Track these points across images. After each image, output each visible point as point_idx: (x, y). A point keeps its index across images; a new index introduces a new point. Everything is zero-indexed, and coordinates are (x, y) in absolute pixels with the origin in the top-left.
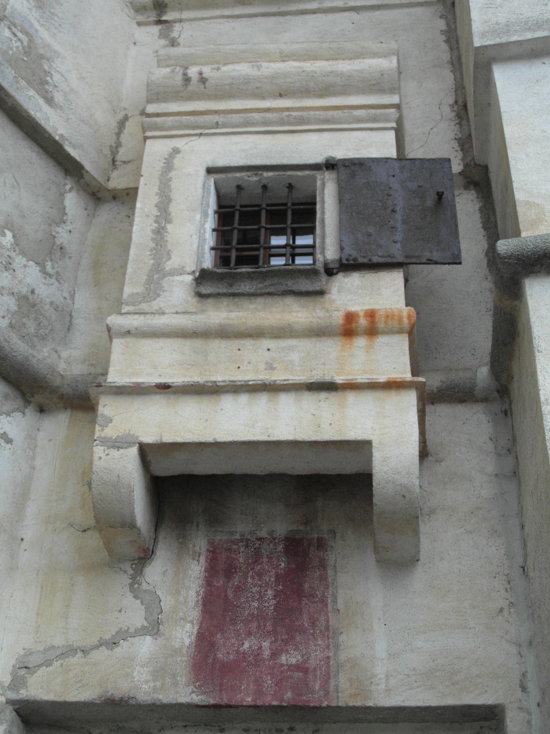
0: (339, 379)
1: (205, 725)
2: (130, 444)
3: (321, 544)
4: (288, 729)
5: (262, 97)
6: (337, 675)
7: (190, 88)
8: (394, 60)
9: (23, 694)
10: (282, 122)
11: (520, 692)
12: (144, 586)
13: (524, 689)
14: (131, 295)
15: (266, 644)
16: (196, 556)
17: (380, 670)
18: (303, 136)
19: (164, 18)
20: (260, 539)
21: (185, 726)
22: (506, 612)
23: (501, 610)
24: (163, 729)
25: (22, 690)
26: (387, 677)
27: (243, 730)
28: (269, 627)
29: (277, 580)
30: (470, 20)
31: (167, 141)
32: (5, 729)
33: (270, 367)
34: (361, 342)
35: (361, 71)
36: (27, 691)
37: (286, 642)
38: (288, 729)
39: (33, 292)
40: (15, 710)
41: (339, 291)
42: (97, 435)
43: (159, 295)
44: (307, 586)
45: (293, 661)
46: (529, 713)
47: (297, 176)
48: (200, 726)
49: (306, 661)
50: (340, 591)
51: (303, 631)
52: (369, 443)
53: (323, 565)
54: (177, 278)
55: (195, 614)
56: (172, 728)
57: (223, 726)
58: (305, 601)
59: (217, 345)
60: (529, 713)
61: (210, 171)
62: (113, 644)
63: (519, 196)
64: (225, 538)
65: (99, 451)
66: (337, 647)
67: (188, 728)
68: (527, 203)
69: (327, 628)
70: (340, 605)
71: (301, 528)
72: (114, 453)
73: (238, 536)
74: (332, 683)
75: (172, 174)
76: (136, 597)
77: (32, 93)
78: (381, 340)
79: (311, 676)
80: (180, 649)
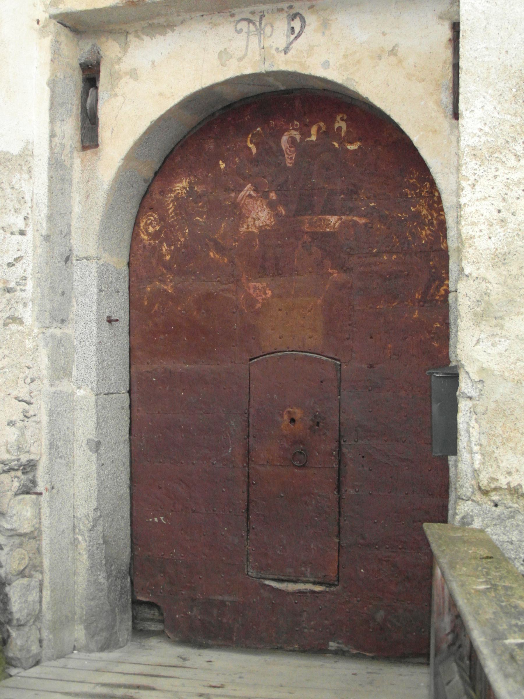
1: (218, 13)
4: (288, 8)
11: (291, 51)
21: (202, 16)
24: (184, 20)
25: (61, 5)
27: (250, 13)
32: (52, 40)
36: (65, 5)
38: (288, 8)
40: (59, 22)
47: (299, 355)
48: (214, 13)
56: (192, 18)
57: (233, 12)
67: (204, 17)
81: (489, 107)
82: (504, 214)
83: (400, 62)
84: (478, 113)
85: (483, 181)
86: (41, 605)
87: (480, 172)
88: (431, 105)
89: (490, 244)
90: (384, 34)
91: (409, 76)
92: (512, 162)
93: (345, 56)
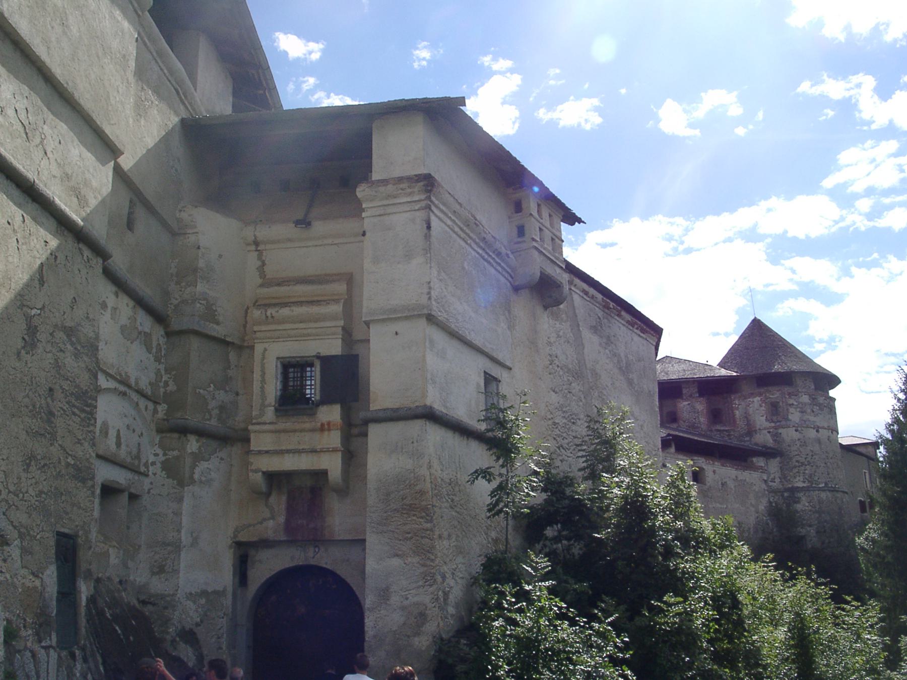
0: (319, 447)
5: (294, 323)
9: (237, 539)
10: (301, 336)
19: (259, 249)
30: (342, 460)
34: (326, 433)
39: (223, 402)
42: (249, 468)
54: (269, 408)
61: (278, 358)
62: (261, 523)
63: (371, 388)
65: (250, 474)
72: (255, 474)
75: (265, 361)
77: (211, 324)
78: (332, 432)
92: (378, 612)
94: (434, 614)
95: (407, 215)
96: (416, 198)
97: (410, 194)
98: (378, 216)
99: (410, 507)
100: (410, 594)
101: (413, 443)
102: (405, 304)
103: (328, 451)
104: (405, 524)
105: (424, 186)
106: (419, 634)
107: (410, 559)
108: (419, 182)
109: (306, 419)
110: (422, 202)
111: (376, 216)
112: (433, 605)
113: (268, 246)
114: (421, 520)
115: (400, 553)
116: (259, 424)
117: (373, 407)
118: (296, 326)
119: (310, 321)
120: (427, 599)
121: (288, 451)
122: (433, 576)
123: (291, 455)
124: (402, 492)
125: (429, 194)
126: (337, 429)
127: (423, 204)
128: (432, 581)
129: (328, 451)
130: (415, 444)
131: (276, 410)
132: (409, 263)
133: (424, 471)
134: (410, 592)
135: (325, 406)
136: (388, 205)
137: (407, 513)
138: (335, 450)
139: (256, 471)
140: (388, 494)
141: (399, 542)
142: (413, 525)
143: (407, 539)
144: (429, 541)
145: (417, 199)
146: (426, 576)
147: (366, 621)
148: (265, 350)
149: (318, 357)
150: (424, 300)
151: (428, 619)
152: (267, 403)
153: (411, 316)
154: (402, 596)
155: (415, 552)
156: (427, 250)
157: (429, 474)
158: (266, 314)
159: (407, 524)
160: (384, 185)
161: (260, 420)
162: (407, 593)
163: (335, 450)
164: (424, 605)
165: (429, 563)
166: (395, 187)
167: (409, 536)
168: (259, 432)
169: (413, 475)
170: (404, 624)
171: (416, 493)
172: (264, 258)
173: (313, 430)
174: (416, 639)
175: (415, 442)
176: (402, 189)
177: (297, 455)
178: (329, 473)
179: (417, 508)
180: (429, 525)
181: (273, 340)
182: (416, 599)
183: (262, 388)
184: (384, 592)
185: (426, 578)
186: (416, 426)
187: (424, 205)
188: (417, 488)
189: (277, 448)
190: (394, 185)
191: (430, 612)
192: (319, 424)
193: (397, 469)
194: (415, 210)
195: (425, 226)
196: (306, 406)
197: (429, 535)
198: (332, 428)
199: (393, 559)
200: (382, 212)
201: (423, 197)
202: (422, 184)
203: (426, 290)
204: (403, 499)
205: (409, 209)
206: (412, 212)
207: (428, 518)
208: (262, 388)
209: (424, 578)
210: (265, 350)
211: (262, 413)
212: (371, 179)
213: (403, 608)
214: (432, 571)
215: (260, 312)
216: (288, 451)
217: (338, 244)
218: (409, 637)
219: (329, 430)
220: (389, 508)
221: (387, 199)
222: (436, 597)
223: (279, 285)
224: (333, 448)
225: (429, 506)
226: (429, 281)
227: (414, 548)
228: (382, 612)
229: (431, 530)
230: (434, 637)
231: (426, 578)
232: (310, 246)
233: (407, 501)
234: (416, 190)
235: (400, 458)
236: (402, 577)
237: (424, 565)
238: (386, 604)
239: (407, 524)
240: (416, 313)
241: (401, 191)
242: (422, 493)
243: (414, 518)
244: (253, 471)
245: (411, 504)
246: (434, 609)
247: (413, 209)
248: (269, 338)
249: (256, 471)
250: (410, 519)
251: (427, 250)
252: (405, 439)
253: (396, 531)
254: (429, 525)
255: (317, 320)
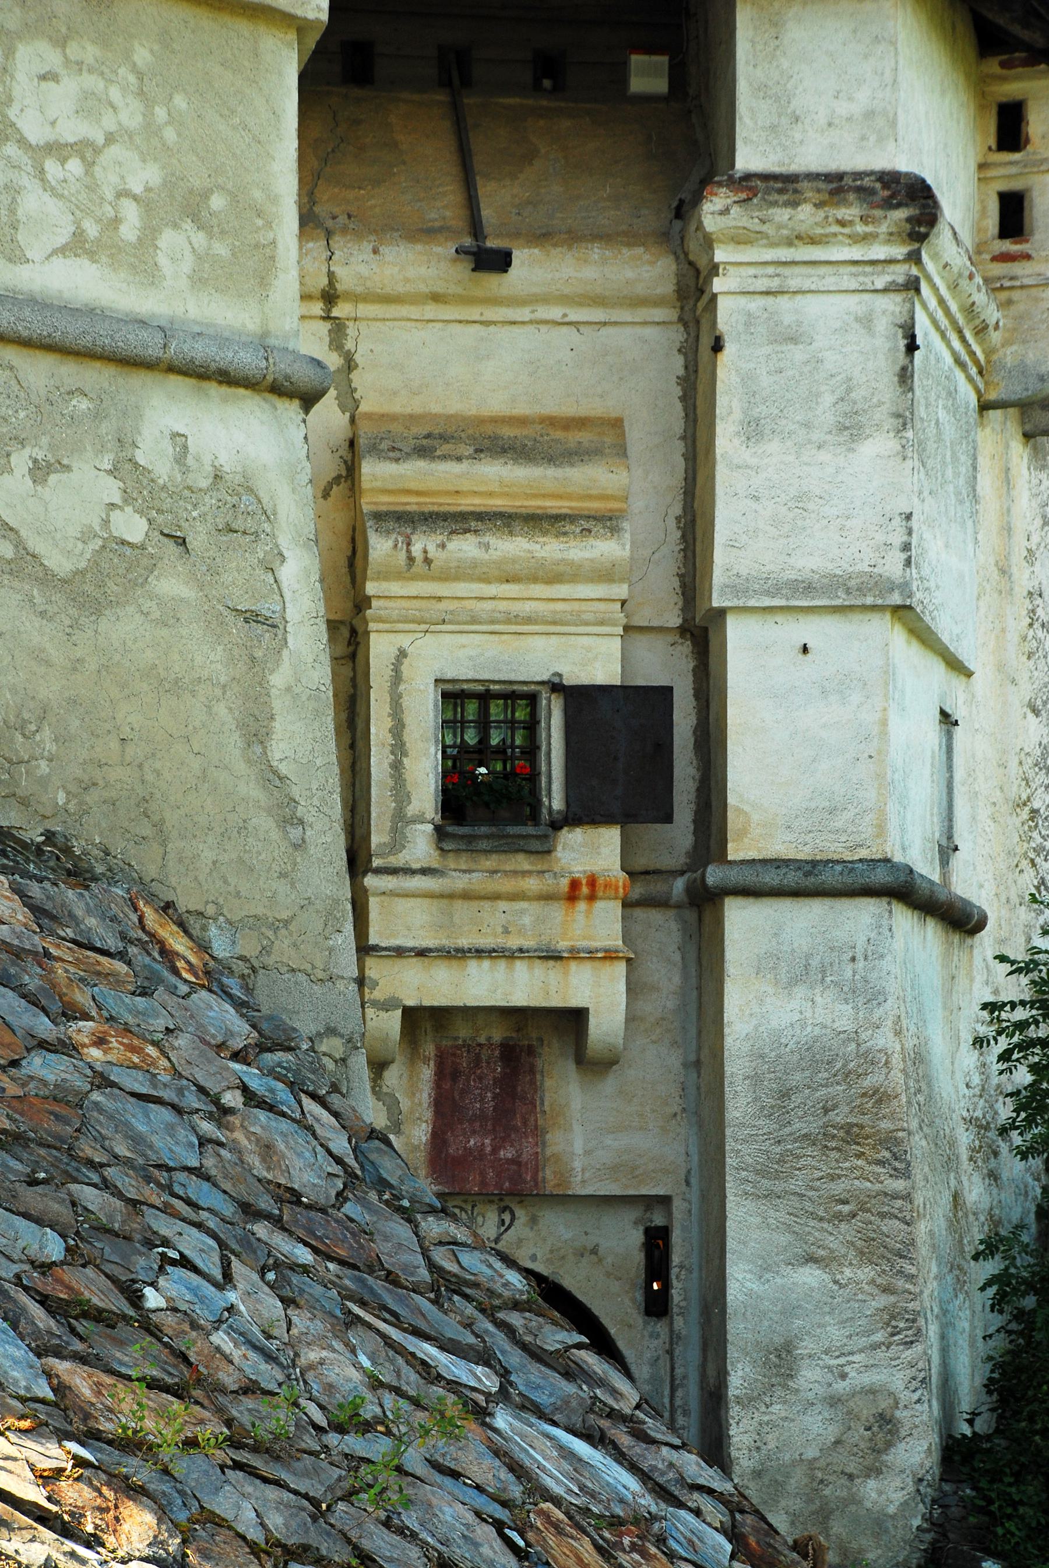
0: (563, 945)
2: (396, 1008)
3: (531, 1051)
5: (486, 580)
6: (543, 1169)
7: (414, 569)
8: (625, 586)
10: (508, 621)
12: (385, 1089)
13: (688, 1183)
14: (379, 845)
15: (487, 1141)
16: (426, 1060)
17: (577, 1165)
18: (530, 638)
19: (335, 313)
20: (480, 1045)
22: (679, 1118)
23: (675, 1115)
26: (583, 1170)
28: (490, 1127)
29: (495, 1083)
31: (392, 636)
33: (506, 931)
34: (582, 906)
35: (592, 560)
37: (504, 1140)
41: (564, 849)
43: (404, 847)
44: (519, 1089)
45: (509, 1156)
46: (690, 1203)
49: (519, 1156)
50: (547, 1094)
51: (516, 1130)
52: (587, 1009)
53: (532, 1071)
54: (419, 827)
55: (429, 1115)
58: (518, 1103)
59: (459, 904)
60: (690, 1203)
63: (731, 800)
64: (450, 1043)
65: (370, 1012)
66: (544, 1144)
68: (738, 810)
69: (536, 1127)
70: (547, 1108)
71: (514, 1035)
73: (460, 1042)
74: (540, 1174)
75: (402, 688)
76: (378, 1099)
78: (600, 905)
79: (523, 1169)
80: (419, 1146)
81: (747, 1370)
82: (758, 1444)
83: (600, 1260)
84: (740, 1373)
85: (744, 1421)
86: (690, 1510)
87: (742, 1414)
88: (627, 1302)
89: (751, 1463)
90: (586, 1233)
91: (608, 1274)
92: (763, 1409)
93: (551, 1251)
94: (917, 1421)
95: (852, 302)
96: (880, 252)
97: (865, 239)
98: (762, 293)
99: (848, 1132)
100: (849, 1363)
101: (853, 959)
102: (839, 572)
103: (590, 955)
104: (833, 1178)
105: (909, 220)
106: (879, 1472)
107: (848, 1272)
108: (899, 206)
109: (522, 862)
110: (892, 268)
111: (754, 293)
112: (916, 1396)
113: (365, 310)
114: (879, 1169)
115: (822, 1253)
116: (393, 871)
117: (735, 851)
118: (492, 590)
119: (534, 579)
120: (898, 1381)
121: (479, 953)
122: (914, 1321)
123: (486, 964)
124: (822, 1092)
125: (916, 245)
126: (616, 898)
127: (899, 273)
128: (910, 1332)
129: (590, 955)
130: (861, 964)
131: (440, 833)
132: (853, 450)
133: (884, 1039)
134: (850, 1358)
135: (578, 830)
136: (794, 263)
137: (838, 1149)
138: (610, 956)
139: (386, 1006)
140: (785, 1094)
141: (818, 1225)
142: (856, 1182)
143: (839, 1217)
144: (903, 1226)
145: (882, 257)
146: (893, 1317)
147: (731, 1433)
148: (402, 654)
149: (556, 687)
150: (892, 566)
151: (903, 1433)
152: (411, 810)
153: (851, 608)
154: (829, 1367)
155: (862, 1253)
156: (903, 420)
157: (898, 1048)
158: (408, 551)
159: (839, 1177)
160: (786, 204)
161: (395, 861)
162: (842, 1360)
163: (610, 956)
164: (891, 1394)
165: (901, 1283)
166: (821, 214)
167: (846, 1209)
168: (393, 894)
169: (853, 1046)
170: (838, 1442)
171: (864, 1095)
172: (349, 345)
173: (547, 897)
174: (872, 1484)
175: (860, 957)
176: (842, 223)
177: (502, 964)
178: (593, 1021)
179: (867, 1137)
180: (899, 1185)
181: (424, 627)
182: (868, 1379)
183: (397, 766)
184: (779, 1356)
185: (893, 1323)
186: (867, 911)
187: (901, 280)
188: (867, 1082)
189: (446, 942)
190: (818, 206)
191: (905, 1413)
192: (564, 883)
193: (809, 1029)
194: (876, 291)
195: (902, 343)
196: (530, 830)
197: (901, 1210)
198: (600, 894)
199: (801, 1270)
200: (774, 284)
201: (899, 251)
202: (901, 214)
203: (898, 538)
204: (826, 1111)
205: (854, 285)
206: (866, 297)
207: (897, 1164)
208: (397, 766)
209: (888, 1325)
210: (402, 654)
211: (397, 843)
212: (732, 165)
213: (834, 1401)
214: (911, 1306)
215: (390, 543)
216: (479, 953)
217: (578, 323)
218: (851, 1477)
219: (592, 898)
220: (787, 1130)
221: (790, 244)
222: (922, 1375)
223: (423, 453)
224: (606, 951)
225: (900, 1134)
226: (908, 511)
227: (860, 1243)
228: (776, 1408)
229: (908, 1197)
230: (921, 1480)
231: (893, 1323)
232: (494, 323)
233: (839, 1117)
234: (883, 228)
235: (818, 999)
236: (827, 1318)
237: (887, 1290)
238: (785, 1386)
239: (839, 1177)
240: (869, 601)
241: (835, 228)
242: (880, 1097)
243: (860, 1162)
244: (376, 1004)
245: (852, 1125)
246: (918, 1406)
247: (870, 287)
248: (413, 621)
249: (386, 1006)
250: (847, 1164)
251: (903, 420)
252: (832, 949)
253: (811, 1193)
254: (899, 1185)
255: (555, 578)
